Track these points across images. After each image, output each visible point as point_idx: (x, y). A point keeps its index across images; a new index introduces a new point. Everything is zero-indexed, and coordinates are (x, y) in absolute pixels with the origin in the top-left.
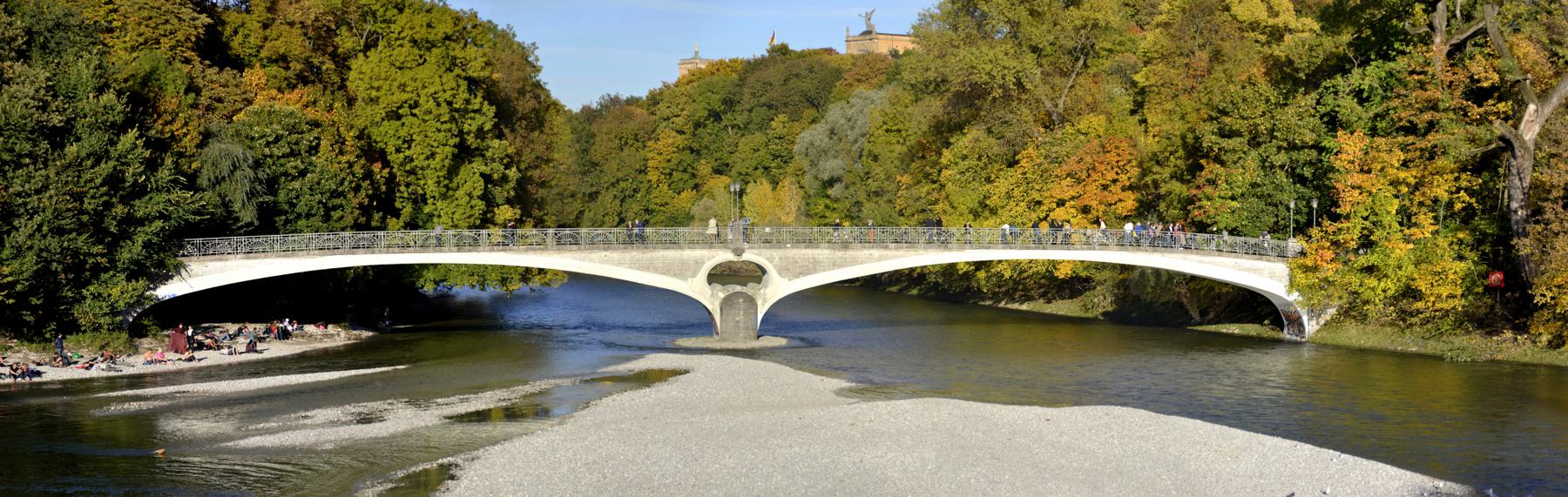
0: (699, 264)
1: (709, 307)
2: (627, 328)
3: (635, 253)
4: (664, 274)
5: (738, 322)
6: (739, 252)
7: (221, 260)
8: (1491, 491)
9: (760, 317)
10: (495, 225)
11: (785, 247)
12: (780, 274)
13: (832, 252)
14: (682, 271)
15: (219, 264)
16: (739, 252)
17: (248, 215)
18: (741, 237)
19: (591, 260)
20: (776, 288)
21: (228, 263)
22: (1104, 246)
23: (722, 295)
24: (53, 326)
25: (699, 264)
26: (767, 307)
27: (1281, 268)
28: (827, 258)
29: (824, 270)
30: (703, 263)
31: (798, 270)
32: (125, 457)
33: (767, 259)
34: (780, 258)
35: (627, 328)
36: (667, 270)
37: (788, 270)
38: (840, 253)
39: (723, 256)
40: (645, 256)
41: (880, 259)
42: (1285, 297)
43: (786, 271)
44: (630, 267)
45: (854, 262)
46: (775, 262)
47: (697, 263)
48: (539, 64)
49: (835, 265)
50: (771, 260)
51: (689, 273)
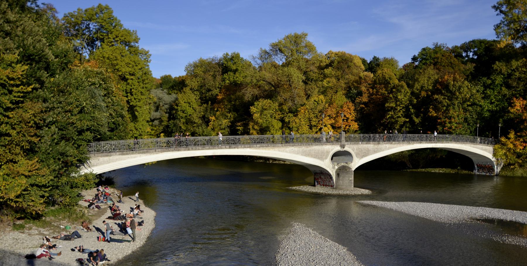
0: (328, 152)
1: (331, 173)
3: (304, 148)
4: (315, 158)
5: (351, 180)
6: (343, 146)
7: (107, 156)
10: (45, 107)
11: (359, 144)
12: (357, 156)
13: (374, 146)
15: (106, 158)
16: (343, 146)
17: (289, 152)
19: (286, 152)
20: (356, 163)
21: (111, 158)
23: (336, 167)
27: (490, 148)
28: (372, 149)
29: (371, 154)
33: (352, 149)
34: (357, 149)
37: (359, 154)
38: (376, 146)
39: (337, 148)
40: (308, 149)
41: (389, 149)
42: (491, 159)
44: (302, 155)
45: (381, 150)
46: (355, 151)
48: (226, 53)
49: (375, 152)
50: (353, 150)
51: (324, 157)
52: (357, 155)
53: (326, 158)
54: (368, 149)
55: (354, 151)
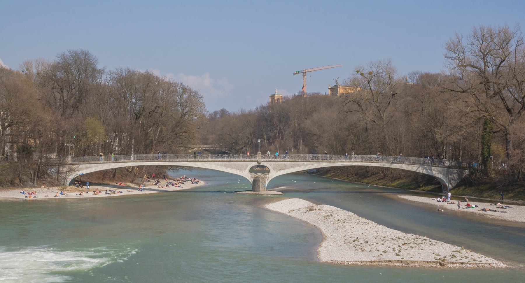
2: (220, 192)
8: (124, 267)
9: (267, 184)
14: (241, 169)
18: (261, 158)
19: (211, 164)
20: (273, 174)
22: (134, 167)
24: (468, 166)
25: (247, 166)
26: (269, 180)
30: (248, 166)
31: (280, 169)
32: (246, 251)
35: (220, 192)
36: (236, 168)
37: (276, 168)
41: (307, 165)
43: (275, 169)
46: (272, 166)
47: (246, 166)
51: (243, 169)
52: (274, 169)
53: (245, 170)
54: (285, 164)
55: (271, 166)
